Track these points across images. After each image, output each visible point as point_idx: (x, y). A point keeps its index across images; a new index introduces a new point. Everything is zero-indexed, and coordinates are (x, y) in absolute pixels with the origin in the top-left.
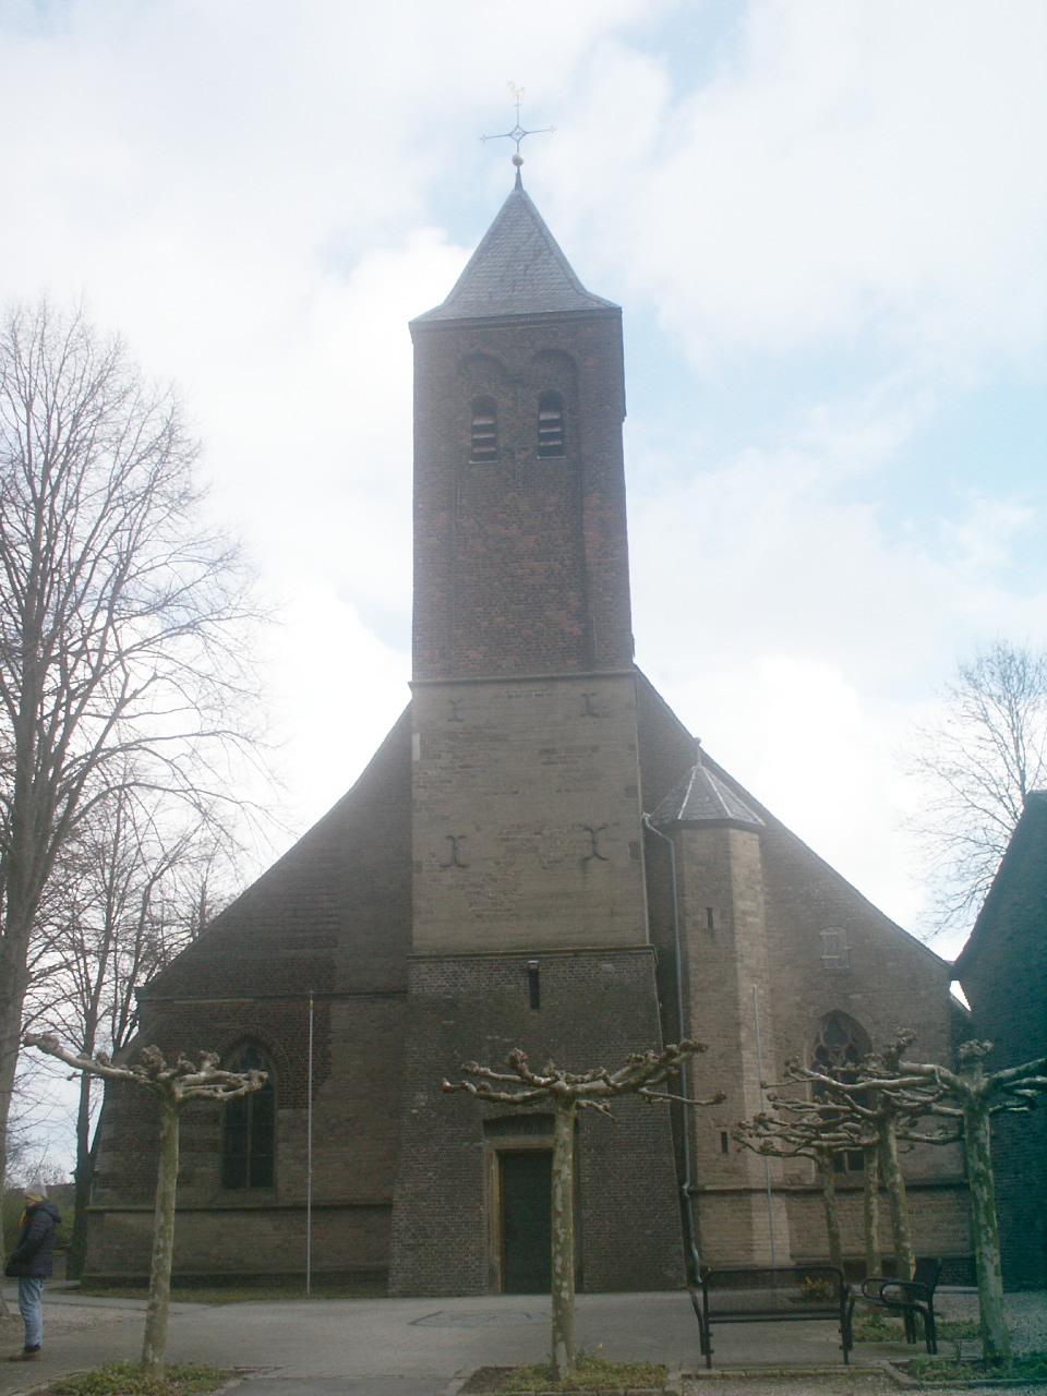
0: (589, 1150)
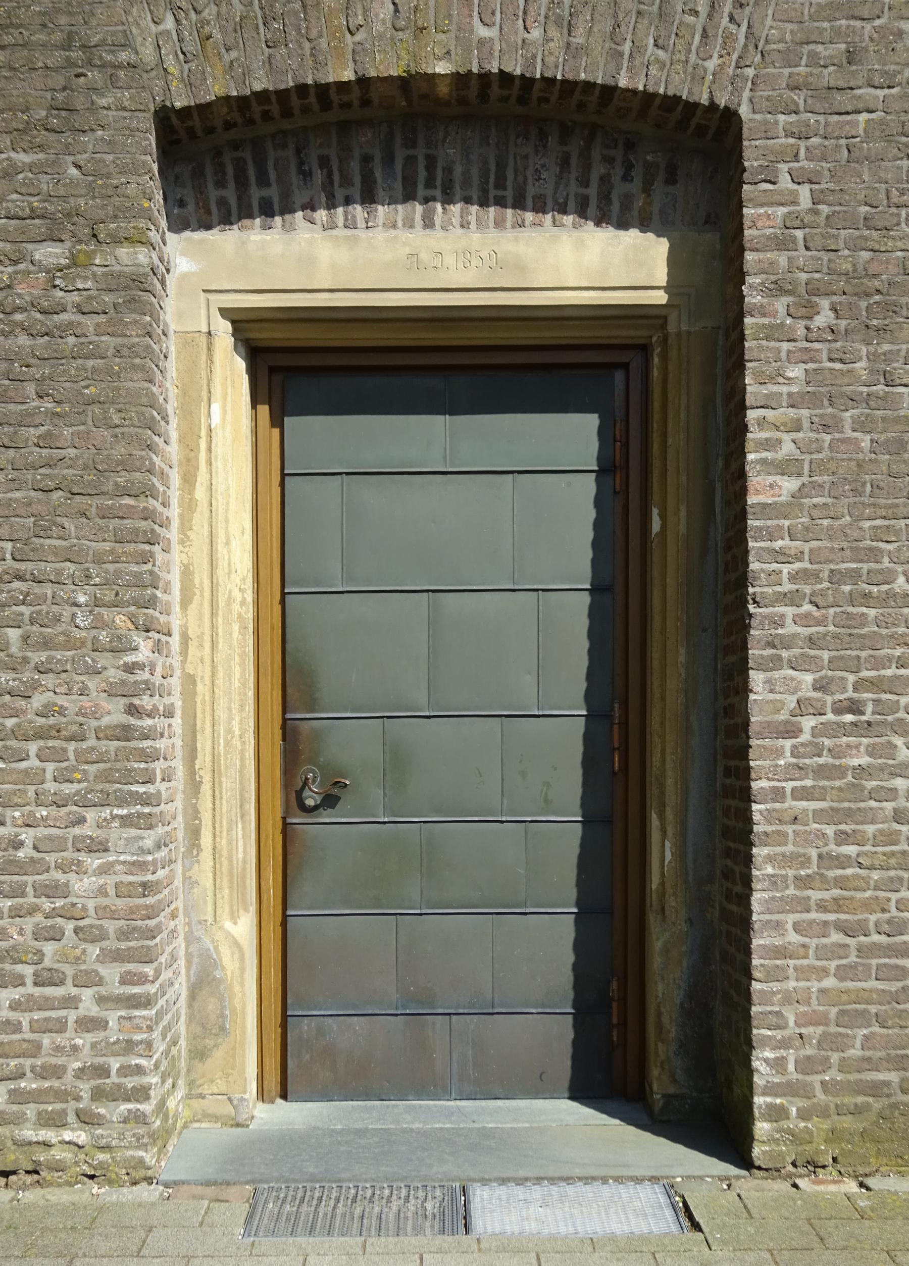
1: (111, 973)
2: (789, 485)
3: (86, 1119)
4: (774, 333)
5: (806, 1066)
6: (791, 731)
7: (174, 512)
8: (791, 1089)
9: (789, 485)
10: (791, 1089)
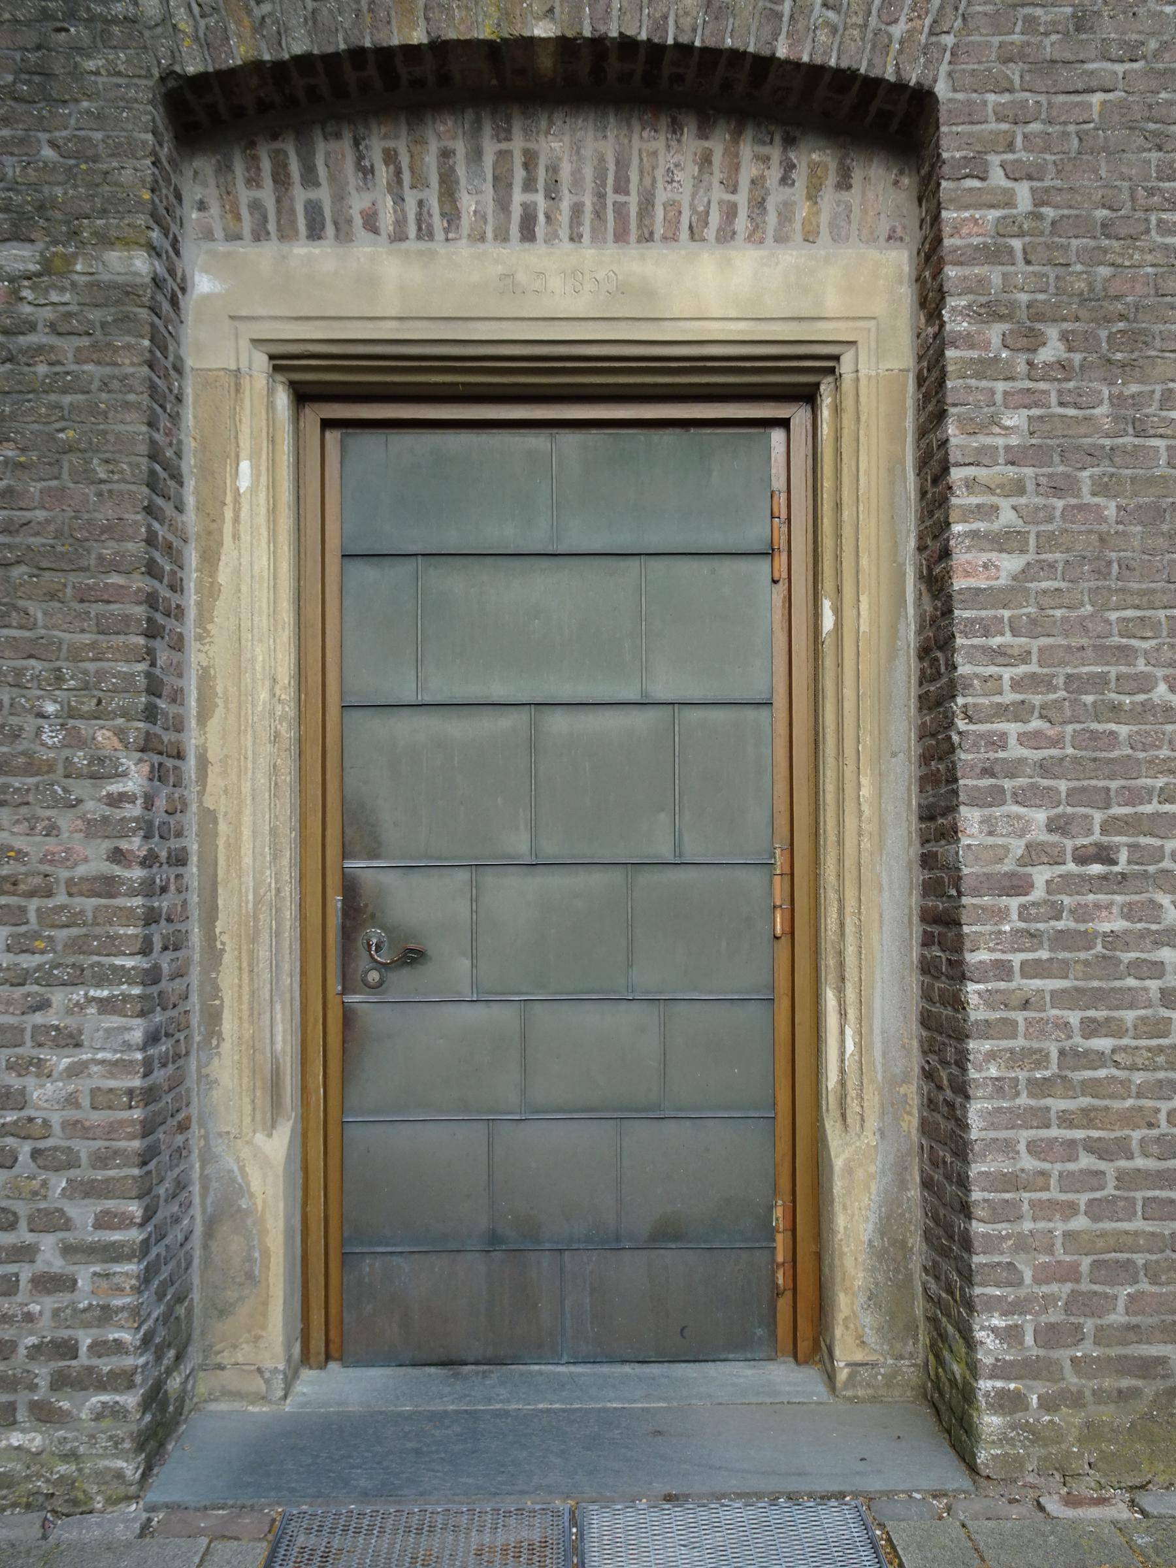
0: (1032, 340)
1: (83, 1213)
2: (1010, 564)
3: (44, 1415)
4: (986, 368)
5: (1049, 1336)
6: (1017, 885)
7: (191, 599)
8: (1027, 1369)
9: (1010, 564)
10: (1027, 1369)
